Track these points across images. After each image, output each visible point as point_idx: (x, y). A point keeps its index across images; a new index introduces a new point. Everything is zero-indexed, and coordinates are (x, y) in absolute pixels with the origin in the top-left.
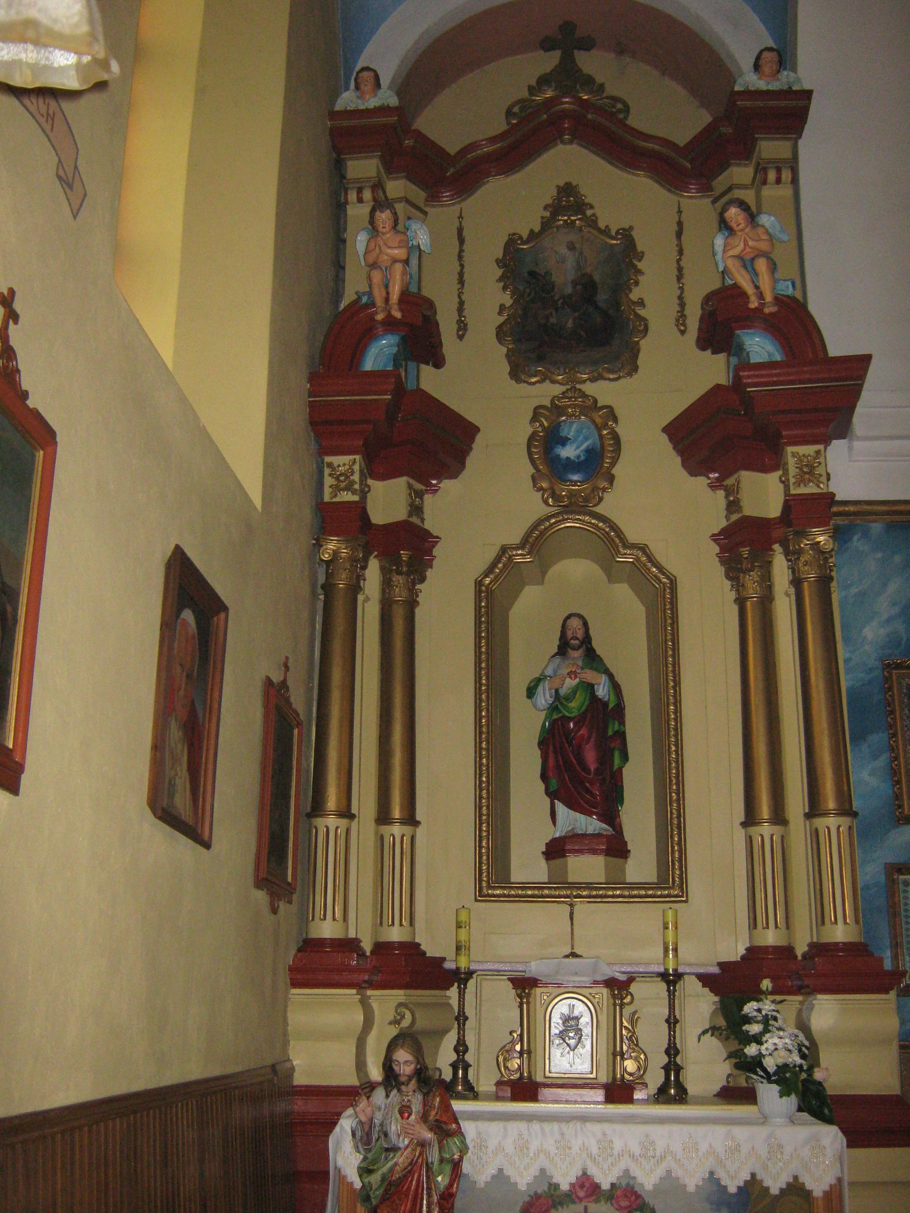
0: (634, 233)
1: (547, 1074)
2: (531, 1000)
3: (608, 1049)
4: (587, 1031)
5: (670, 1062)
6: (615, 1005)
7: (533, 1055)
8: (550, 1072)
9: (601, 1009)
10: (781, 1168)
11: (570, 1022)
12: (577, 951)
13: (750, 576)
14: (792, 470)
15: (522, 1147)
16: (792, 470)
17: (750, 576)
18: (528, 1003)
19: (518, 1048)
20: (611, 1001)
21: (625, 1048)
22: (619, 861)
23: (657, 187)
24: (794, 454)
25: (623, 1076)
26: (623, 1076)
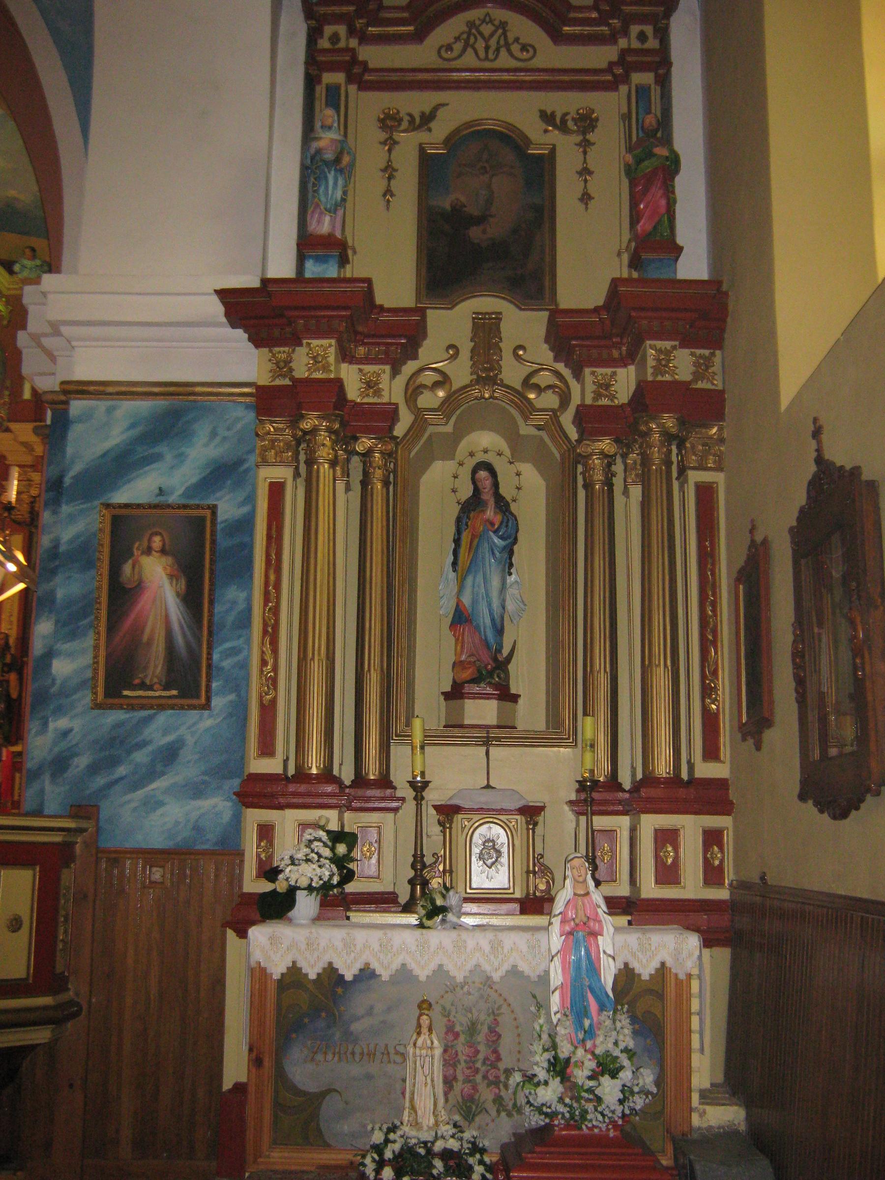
0: (580, 196)
1: (468, 891)
2: (454, 826)
3: (522, 868)
4: (504, 850)
5: (416, 875)
6: (528, 829)
7: (454, 875)
8: (471, 888)
9: (517, 831)
10: (355, 958)
11: (490, 845)
12: (492, 784)
13: (696, 433)
14: (651, 363)
15: (348, 945)
16: (651, 363)
17: (696, 433)
18: (450, 828)
19: (441, 868)
20: (525, 826)
21: (537, 869)
22: (509, 704)
23: (674, 117)
24: (651, 349)
25: (534, 893)
26: (534, 893)
